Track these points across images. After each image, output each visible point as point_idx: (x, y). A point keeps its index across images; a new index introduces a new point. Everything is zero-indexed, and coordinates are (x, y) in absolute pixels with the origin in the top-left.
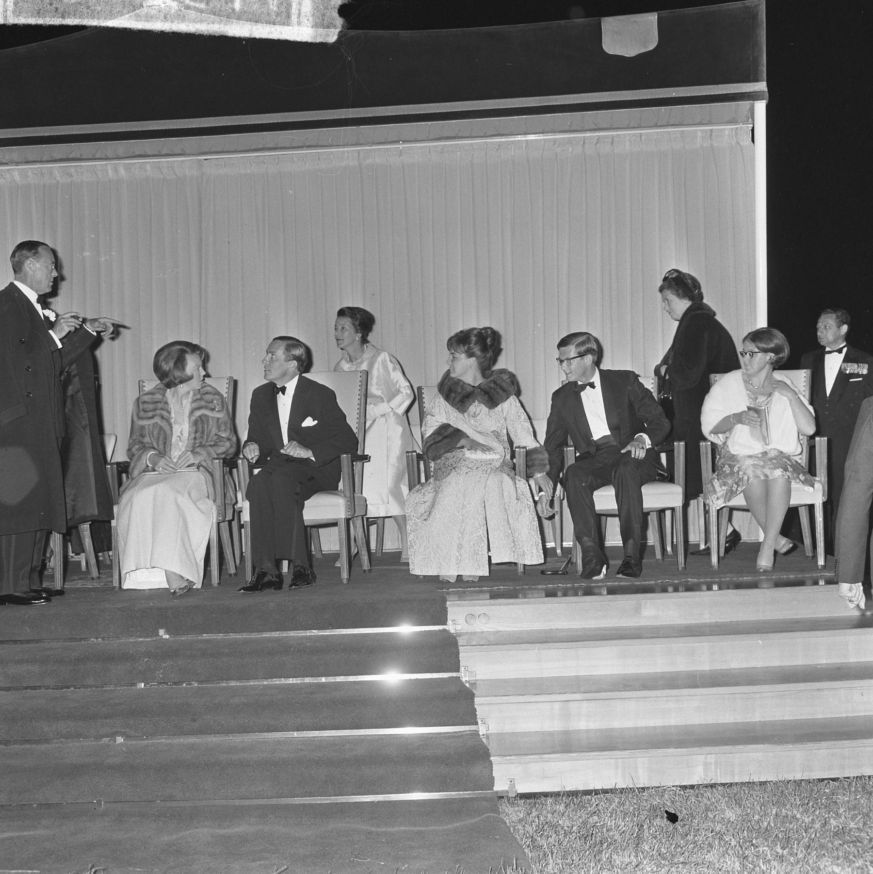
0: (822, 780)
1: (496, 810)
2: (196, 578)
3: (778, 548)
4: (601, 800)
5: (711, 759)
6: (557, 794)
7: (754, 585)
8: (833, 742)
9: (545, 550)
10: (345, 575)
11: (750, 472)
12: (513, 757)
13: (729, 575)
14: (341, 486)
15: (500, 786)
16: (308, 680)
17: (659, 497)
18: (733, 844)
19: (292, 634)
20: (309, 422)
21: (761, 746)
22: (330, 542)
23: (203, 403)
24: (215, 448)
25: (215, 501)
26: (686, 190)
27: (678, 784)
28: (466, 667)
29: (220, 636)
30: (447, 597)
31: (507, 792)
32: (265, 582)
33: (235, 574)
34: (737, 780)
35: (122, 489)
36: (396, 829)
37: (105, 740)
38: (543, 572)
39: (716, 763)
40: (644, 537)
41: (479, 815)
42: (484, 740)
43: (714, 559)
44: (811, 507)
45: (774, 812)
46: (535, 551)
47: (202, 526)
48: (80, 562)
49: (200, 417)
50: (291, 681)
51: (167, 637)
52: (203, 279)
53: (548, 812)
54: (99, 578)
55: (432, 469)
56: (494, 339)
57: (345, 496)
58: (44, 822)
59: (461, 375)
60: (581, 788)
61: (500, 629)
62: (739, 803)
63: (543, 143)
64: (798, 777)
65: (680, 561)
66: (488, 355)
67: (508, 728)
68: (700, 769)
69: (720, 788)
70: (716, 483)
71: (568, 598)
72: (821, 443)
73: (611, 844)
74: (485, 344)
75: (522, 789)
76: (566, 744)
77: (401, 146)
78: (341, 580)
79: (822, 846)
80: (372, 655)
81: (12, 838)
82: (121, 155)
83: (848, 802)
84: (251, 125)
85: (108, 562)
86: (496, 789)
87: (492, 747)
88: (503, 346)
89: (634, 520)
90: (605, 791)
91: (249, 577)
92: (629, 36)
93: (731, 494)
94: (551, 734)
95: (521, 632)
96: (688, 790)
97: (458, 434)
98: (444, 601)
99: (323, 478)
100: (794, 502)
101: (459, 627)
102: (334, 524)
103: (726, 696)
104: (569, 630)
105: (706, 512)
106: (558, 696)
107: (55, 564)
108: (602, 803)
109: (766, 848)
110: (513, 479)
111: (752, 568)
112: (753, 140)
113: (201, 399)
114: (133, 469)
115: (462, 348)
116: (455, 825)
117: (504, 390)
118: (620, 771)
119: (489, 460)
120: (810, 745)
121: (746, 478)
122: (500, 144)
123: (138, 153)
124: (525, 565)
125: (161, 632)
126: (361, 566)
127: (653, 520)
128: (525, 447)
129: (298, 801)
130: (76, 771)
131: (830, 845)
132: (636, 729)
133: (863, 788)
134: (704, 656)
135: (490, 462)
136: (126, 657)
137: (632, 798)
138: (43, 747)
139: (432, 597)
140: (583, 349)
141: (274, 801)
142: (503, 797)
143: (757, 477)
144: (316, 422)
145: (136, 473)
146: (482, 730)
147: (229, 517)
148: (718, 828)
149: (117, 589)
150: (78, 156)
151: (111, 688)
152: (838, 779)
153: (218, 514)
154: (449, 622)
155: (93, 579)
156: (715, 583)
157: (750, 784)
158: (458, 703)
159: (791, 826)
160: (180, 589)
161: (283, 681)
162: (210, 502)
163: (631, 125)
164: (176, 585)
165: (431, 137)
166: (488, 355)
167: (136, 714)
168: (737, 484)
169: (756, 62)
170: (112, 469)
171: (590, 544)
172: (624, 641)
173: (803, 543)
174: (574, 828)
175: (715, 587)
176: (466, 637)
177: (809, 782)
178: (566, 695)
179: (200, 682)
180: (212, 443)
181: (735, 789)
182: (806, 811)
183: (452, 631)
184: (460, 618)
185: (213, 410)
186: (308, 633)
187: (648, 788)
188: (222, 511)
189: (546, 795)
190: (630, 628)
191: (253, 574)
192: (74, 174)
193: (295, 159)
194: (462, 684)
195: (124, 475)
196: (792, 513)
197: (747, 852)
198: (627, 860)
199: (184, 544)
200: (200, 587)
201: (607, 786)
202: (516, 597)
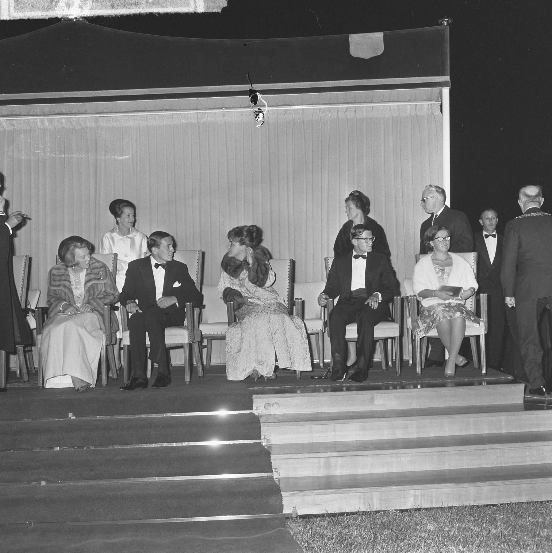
1: (284, 525)
2: (92, 381)
3: (458, 363)
4: (350, 519)
5: (418, 493)
6: (322, 516)
7: (443, 385)
8: (493, 482)
9: (313, 364)
10: (187, 379)
11: (441, 315)
12: (295, 492)
13: (428, 379)
14: (185, 323)
16: (165, 445)
18: (432, 545)
19: (154, 416)
22: (178, 359)
24: (103, 300)
26: (403, 140)
27: (398, 508)
28: (265, 436)
29: (108, 417)
31: (291, 514)
32: (137, 382)
33: (117, 379)
34: (434, 506)
35: (44, 324)
36: (221, 538)
37: (34, 483)
38: (312, 378)
39: (421, 496)
40: (372, 357)
42: (277, 482)
43: (419, 370)
44: (478, 337)
45: (458, 525)
47: (95, 348)
48: (16, 371)
50: (154, 445)
51: (74, 418)
52: (98, 193)
53: (317, 527)
54: (28, 381)
56: (257, 234)
59: (237, 255)
60: (338, 512)
63: (312, 110)
64: (472, 504)
65: (397, 370)
66: (254, 244)
67: (292, 474)
68: (412, 499)
70: (420, 322)
72: (484, 297)
73: (357, 545)
74: (252, 235)
75: (301, 512)
76: (328, 484)
77: (224, 111)
78: (185, 382)
79: (488, 546)
82: (46, 113)
83: (503, 518)
85: (34, 372)
86: (284, 512)
87: (282, 486)
88: (263, 238)
89: (366, 344)
90: (353, 513)
91: (126, 381)
92: (366, 44)
93: (429, 328)
94: (318, 478)
95: (299, 414)
96: (404, 513)
99: (174, 318)
100: (467, 334)
101: (260, 411)
102: (181, 347)
103: (434, 453)
104: (329, 413)
105: (413, 341)
106: (323, 454)
108: (351, 521)
109: (453, 547)
111: (442, 375)
112: (441, 111)
114: (51, 312)
115: (238, 239)
116: (259, 535)
118: (362, 501)
120: (479, 484)
121: (438, 318)
122: (286, 111)
123: (56, 112)
124: (301, 372)
125: (70, 415)
128: (301, 299)
129: (159, 521)
131: (492, 545)
132: (372, 474)
133: (512, 510)
134: (413, 429)
137: (370, 517)
142: (288, 518)
143: (445, 317)
145: (52, 315)
146: (275, 476)
148: (423, 535)
149: (41, 388)
150: (18, 113)
151: (38, 450)
152: (496, 505)
154: (254, 408)
155: (24, 382)
156: (419, 384)
157: (442, 509)
158: (261, 458)
160: (82, 387)
161: (149, 445)
163: (367, 101)
165: (243, 106)
166: (254, 244)
168: (433, 322)
171: (339, 359)
172: (362, 420)
173: (473, 361)
174: (334, 536)
175: (419, 386)
176: (264, 418)
177: (478, 507)
178: (326, 453)
179: (96, 446)
180: (102, 296)
181: (433, 512)
182: (477, 525)
183: (256, 414)
186: (165, 415)
187: (379, 511)
189: (315, 516)
190: (367, 412)
191: (129, 379)
192: (15, 125)
193: (157, 118)
194: (263, 447)
195: (45, 315)
196: (466, 341)
197: (441, 550)
199: (83, 359)
200: (94, 386)
201: (348, 510)
202: (295, 392)
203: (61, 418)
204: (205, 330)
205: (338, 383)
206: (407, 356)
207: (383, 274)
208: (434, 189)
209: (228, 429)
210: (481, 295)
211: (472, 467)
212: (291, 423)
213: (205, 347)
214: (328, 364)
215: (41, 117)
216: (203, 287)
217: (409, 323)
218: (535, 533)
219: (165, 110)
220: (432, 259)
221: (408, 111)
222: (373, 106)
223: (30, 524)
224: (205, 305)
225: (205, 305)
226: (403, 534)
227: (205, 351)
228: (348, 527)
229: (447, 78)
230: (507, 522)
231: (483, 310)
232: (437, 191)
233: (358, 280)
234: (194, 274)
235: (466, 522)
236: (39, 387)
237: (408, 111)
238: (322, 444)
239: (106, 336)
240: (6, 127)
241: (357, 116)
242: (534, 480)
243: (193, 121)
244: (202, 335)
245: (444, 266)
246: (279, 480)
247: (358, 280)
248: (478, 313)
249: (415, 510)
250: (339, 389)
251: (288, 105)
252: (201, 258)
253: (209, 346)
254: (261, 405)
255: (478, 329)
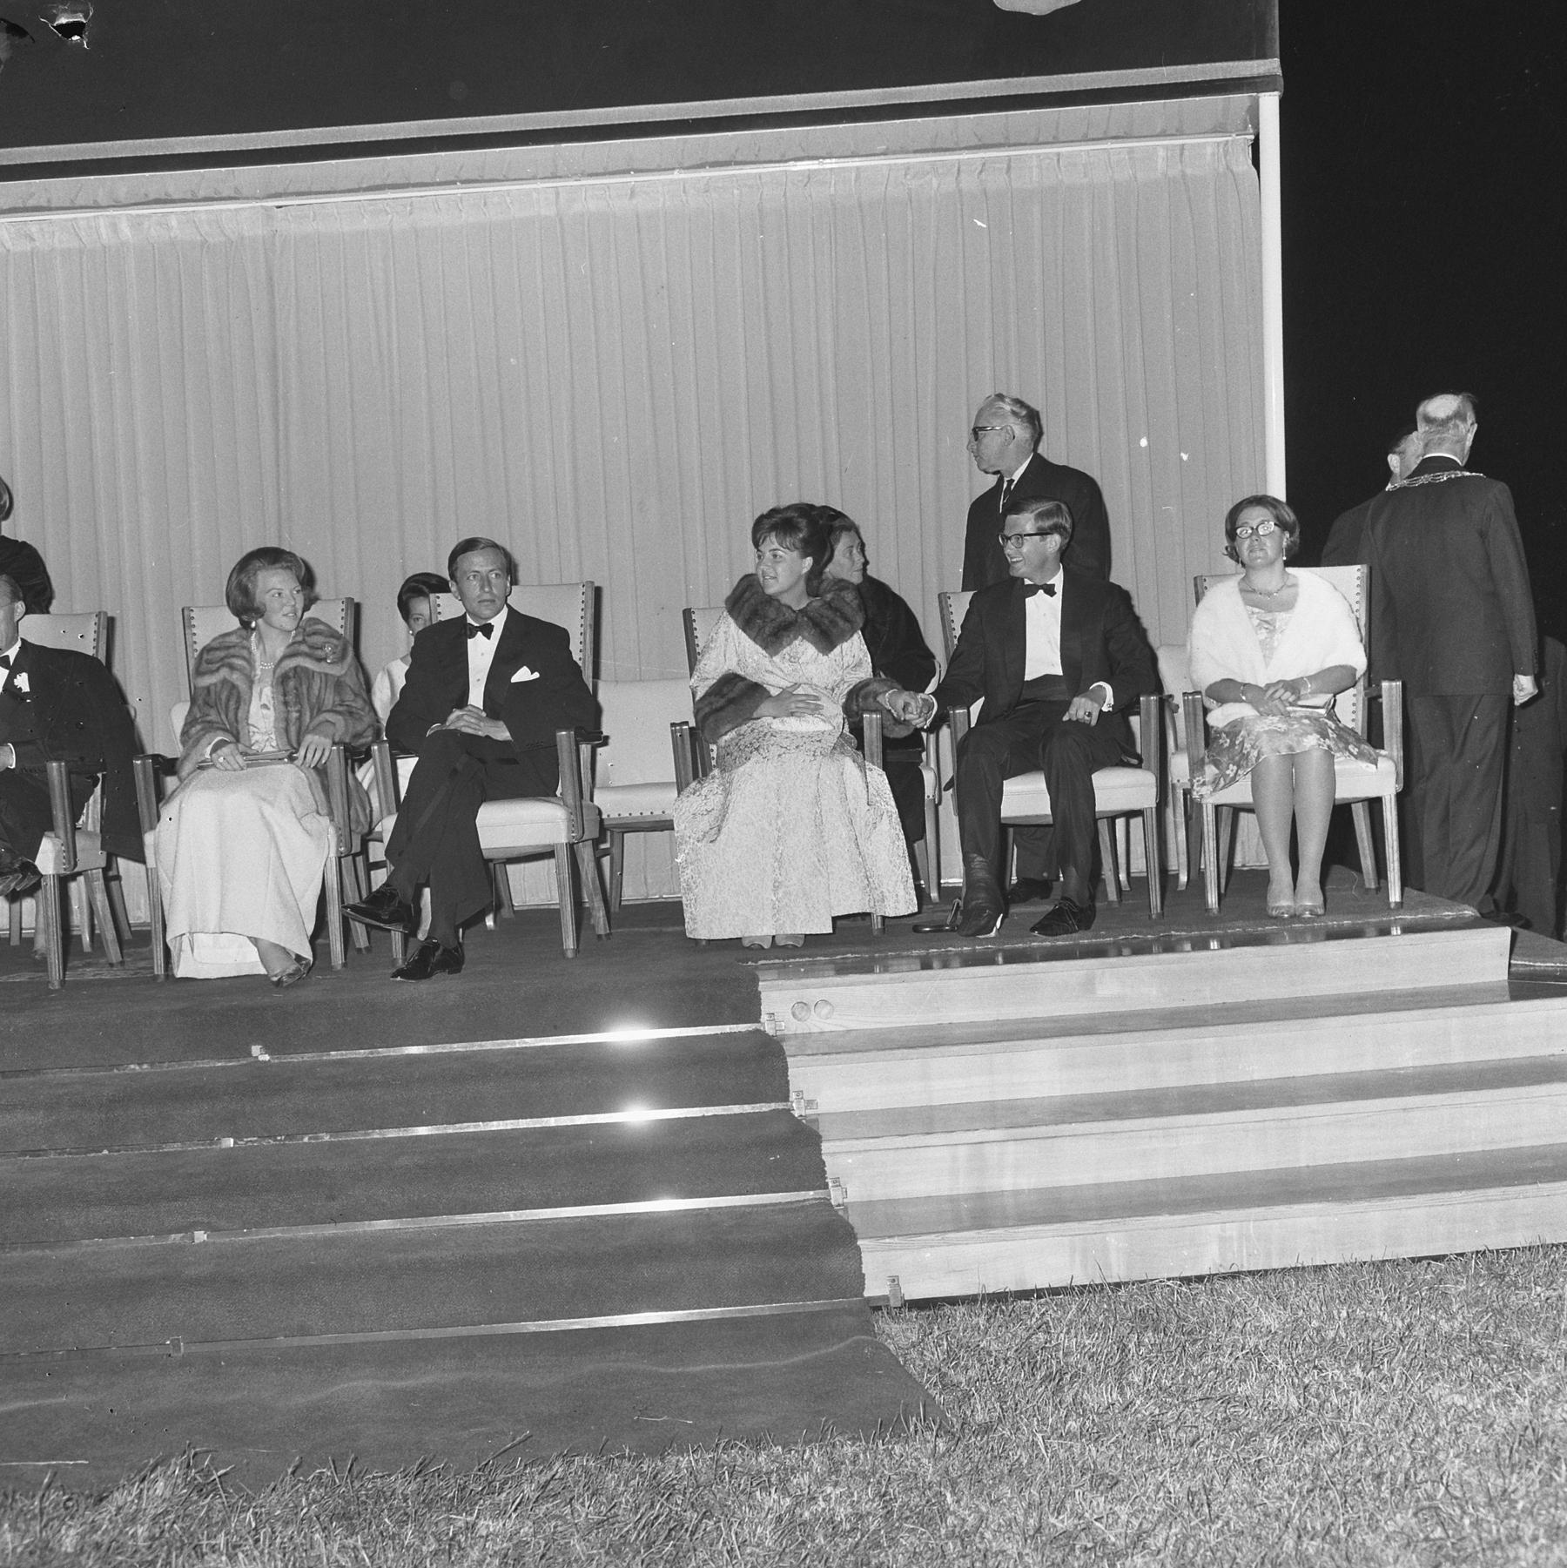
0: (1416, 1260)
1: (867, 1328)
5: (1232, 1230)
8: (1436, 1196)
9: (921, 894)
10: (569, 943)
13: (1240, 923)
15: (874, 1288)
17: (1118, 789)
19: (489, 1045)
20: (523, 675)
21: (1316, 1206)
22: (534, 888)
23: (304, 648)
25: (331, 814)
29: (362, 1053)
30: (759, 973)
31: (886, 1298)
37: (175, 1238)
38: (916, 929)
41: (842, 1340)
43: (1212, 899)
44: (1374, 804)
45: (1344, 1314)
46: (902, 893)
49: (295, 668)
50: (495, 1126)
51: (267, 1057)
54: (122, 963)
55: (714, 755)
57: (565, 805)
58: (78, 1381)
60: (1013, 1288)
61: (853, 1026)
62: (1282, 1300)
64: (1378, 1257)
67: (879, 1193)
69: (1249, 1279)
71: (950, 972)
72: (1391, 690)
73: (1076, 1375)
75: (914, 1291)
76: (981, 1214)
77: (631, 179)
78: (563, 953)
79: (1432, 1365)
80: (604, 1078)
81: (31, 1408)
83: (1465, 1292)
84: (319, 126)
86: (866, 1294)
87: (853, 1220)
90: (1055, 1292)
94: (953, 1199)
95: (891, 1031)
96: (1193, 1285)
97: (755, 691)
98: (755, 980)
99: (527, 774)
100: (1343, 793)
102: (547, 854)
103: (1251, 1126)
107: (47, 941)
110: (862, 768)
112: (1256, 162)
113: (303, 642)
117: (847, 620)
118: (1078, 1258)
119: (817, 733)
121: (1255, 753)
122: (810, 175)
123: (152, 197)
124: (884, 918)
125: (256, 1050)
126: (593, 927)
127: (1103, 826)
129: (532, 1326)
130: (132, 1290)
133: (1489, 1269)
135: (817, 738)
136: (198, 1092)
138: (67, 1253)
139: (722, 976)
140: (1047, 523)
141: (484, 1329)
142: (879, 1308)
144: (536, 675)
145: (184, 774)
146: (835, 1197)
147: (356, 848)
153: (339, 842)
154: (764, 1018)
155: (112, 965)
156: (1213, 937)
158: (795, 1149)
159: (1375, 1336)
162: (325, 821)
164: (281, 968)
167: (228, 1189)
169: (1261, 23)
170: (144, 764)
171: (981, 874)
175: (1214, 944)
177: (1396, 1263)
183: (771, 1032)
184: (783, 1005)
185: (320, 660)
186: (518, 1043)
188: (345, 835)
189: (953, 1301)
190: (1035, 1020)
194: (797, 1122)
196: (1341, 814)
198: (1105, 1399)
201: (1042, 1284)
202: (871, 971)
203: (231, 1058)
204: (610, 804)
205: (981, 942)
206: (1178, 863)
207: (1113, 636)
208: (1008, 408)
209: (669, 1073)
210: (1385, 684)
211: (1366, 1159)
212: (872, 1055)
213: (606, 852)
214: (954, 891)
215: (111, 212)
216: (601, 685)
217: (1179, 766)
218: (1557, 1327)
219: (463, 182)
220: (1242, 591)
221: (1161, 164)
222: (1058, 154)
223: (176, 1346)
224: (607, 738)
225: (607, 738)
226: (1195, 1341)
227: (606, 861)
228: (1044, 1327)
229: (1271, 66)
230: (1477, 1303)
231: (1391, 726)
232: (1014, 413)
233: (1043, 653)
234: (578, 649)
235: (1366, 1303)
236: (156, 977)
237: (1161, 164)
238: (956, 1108)
239: (338, 829)
240: (9, 245)
241: (1140, 175)
242: (1545, 1187)
243: (543, 212)
244: (602, 821)
245: (1267, 606)
246: (846, 1210)
247: (1043, 653)
248: (1374, 735)
249: (1224, 1277)
250: (987, 960)
251: (817, 158)
252: (591, 603)
253: (616, 851)
254: (783, 1005)
255: (1374, 777)
